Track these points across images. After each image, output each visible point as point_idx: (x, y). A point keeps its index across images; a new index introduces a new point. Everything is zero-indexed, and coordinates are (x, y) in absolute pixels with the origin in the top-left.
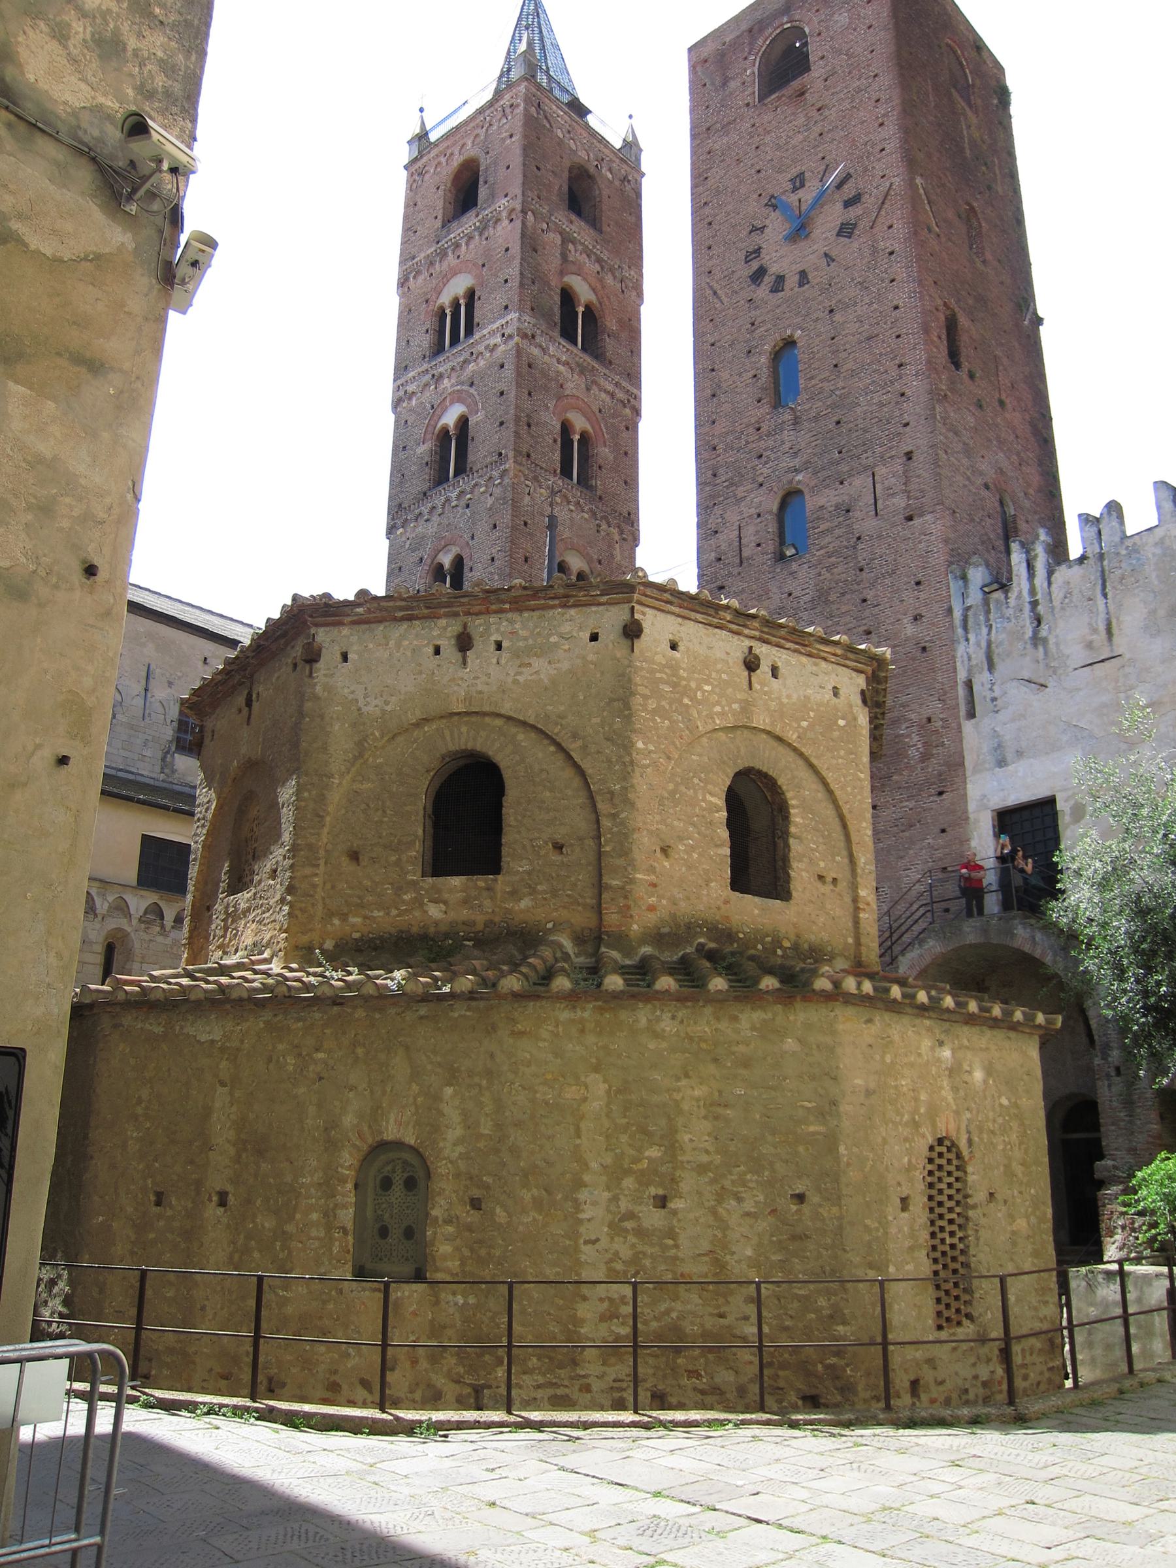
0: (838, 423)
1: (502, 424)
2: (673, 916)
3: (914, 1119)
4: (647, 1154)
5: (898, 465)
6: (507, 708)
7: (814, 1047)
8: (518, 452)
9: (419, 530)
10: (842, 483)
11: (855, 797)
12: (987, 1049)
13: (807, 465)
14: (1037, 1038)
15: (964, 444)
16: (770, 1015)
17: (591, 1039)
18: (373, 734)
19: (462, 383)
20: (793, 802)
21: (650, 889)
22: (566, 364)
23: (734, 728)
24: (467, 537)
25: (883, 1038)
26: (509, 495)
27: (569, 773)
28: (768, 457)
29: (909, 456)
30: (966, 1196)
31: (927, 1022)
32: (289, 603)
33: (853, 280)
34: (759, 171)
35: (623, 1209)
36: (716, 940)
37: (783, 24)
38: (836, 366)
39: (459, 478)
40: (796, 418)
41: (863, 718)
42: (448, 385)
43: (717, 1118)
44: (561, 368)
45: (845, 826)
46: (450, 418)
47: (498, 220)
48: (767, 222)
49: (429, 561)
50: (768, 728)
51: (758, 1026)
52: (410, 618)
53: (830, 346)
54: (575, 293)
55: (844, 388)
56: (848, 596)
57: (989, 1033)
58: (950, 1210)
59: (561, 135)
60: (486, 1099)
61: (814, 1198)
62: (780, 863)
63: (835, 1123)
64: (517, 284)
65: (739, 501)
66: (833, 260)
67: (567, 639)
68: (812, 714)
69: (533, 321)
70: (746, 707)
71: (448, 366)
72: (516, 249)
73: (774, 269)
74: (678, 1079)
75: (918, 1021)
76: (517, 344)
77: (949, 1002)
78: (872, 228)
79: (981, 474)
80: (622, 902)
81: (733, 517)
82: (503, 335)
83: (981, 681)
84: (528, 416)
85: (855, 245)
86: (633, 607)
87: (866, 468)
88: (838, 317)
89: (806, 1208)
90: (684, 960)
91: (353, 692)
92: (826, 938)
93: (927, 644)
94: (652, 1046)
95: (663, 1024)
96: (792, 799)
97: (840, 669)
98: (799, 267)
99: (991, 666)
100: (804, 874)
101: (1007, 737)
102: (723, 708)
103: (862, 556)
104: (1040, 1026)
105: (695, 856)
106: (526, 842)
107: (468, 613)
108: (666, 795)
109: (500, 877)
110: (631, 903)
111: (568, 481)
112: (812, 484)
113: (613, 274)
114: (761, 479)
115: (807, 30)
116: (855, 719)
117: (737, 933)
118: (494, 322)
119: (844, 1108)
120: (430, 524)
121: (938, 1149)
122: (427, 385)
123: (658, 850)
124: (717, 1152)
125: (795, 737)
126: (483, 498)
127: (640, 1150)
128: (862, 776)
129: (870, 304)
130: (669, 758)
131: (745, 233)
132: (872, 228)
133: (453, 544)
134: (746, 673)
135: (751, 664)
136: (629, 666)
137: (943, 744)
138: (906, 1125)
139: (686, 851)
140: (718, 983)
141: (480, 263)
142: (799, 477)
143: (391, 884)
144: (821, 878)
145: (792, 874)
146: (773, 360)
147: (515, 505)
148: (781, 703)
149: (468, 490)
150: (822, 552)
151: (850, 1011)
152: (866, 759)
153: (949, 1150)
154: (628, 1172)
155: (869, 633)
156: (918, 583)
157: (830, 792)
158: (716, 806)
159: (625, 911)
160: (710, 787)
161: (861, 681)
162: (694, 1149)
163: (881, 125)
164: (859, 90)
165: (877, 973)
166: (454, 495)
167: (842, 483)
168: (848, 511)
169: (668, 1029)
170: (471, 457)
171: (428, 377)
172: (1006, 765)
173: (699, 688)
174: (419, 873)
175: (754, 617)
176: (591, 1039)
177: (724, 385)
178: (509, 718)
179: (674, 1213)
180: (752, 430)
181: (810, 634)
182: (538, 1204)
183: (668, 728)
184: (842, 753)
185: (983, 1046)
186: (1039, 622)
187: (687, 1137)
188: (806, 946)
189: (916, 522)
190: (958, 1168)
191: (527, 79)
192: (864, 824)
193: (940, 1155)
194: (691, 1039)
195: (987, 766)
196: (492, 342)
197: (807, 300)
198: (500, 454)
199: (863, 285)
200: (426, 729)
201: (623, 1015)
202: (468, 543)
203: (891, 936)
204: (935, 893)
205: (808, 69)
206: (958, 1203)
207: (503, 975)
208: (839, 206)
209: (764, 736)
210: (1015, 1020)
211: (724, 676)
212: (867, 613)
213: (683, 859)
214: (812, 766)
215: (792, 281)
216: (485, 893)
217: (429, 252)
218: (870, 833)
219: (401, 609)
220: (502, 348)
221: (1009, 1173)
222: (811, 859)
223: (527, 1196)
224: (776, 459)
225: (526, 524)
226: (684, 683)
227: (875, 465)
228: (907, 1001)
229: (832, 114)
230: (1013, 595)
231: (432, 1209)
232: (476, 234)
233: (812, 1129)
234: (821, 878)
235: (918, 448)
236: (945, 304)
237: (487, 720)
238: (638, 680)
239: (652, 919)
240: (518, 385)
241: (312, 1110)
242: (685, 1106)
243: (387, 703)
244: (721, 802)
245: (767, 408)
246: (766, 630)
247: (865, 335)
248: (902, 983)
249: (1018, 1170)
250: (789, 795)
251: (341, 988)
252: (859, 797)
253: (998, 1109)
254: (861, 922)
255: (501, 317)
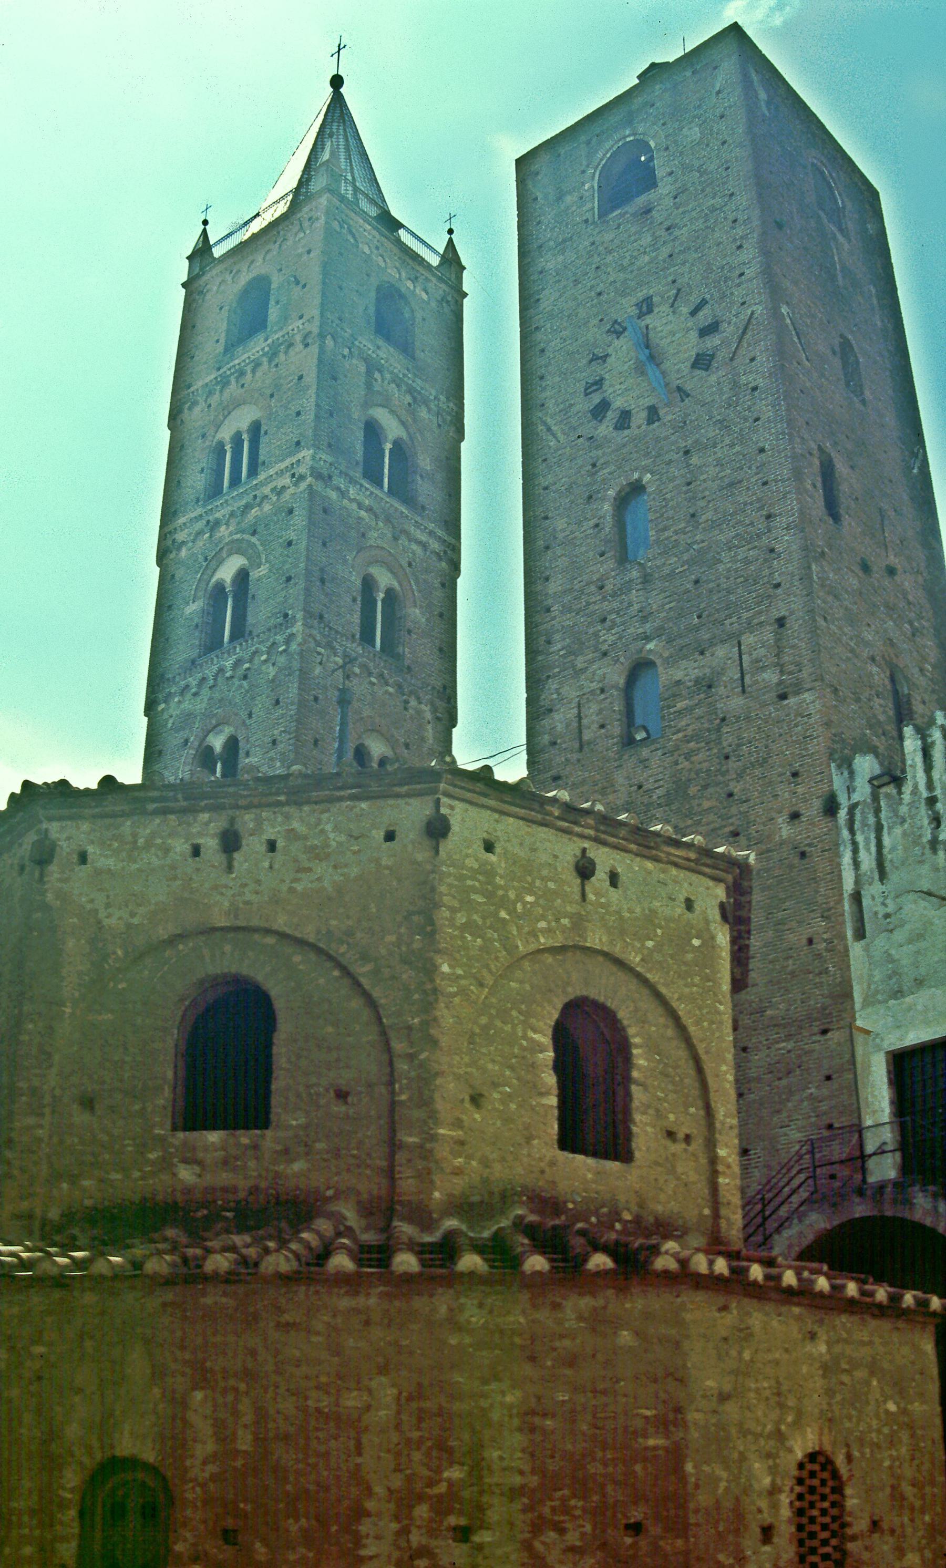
0: (697, 582)
1: (289, 579)
2: (485, 1181)
3: (779, 1431)
4: (446, 1475)
5: (768, 634)
6: (281, 922)
7: (655, 1340)
8: (308, 614)
9: (186, 705)
10: (702, 653)
11: (713, 1034)
12: (871, 1343)
13: (659, 633)
14: (931, 1329)
15: (846, 609)
16: (601, 1302)
17: (377, 1333)
18: (115, 953)
19: (243, 532)
20: (636, 1040)
21: (457, 1148)
22: (369, 510)
23: (563, 949)
24: (243, 714)
25: (741, 1330)
26: (296, 665)
27: (356, 1003)
28: (613, 621)
29: (781, 622)
30: (843, 1525)
31: (796, 1310)
32: (18, 790)
33: (710, 418)
34: (600, 294)
35: (414, 1545)
36: (541, 1213)
37: (625, 137)
38: (693, 515)
39: (235, 643)
40: (645, 576)
41: (723, 938)
42: (227, 533)
43: (533, 1430)
44: (363, 513)
45: (700, 1070)
46: (226, 573)
47: (291, 345)
48: (610, 350)
49: (197, 743)
50: (605, 949)
51: (586, 1315)
52: (164, 812)
53: (686, 493)
54: (381, 427)
55: (703, 541)
56: (711, 790)
57: (873, 1323)
58: (825, 1542)
59: (367, 250)
60: (245, 1406)
61: (655, 1530)
62: (620, 1116)
63: (681, 1435)
64: (312, 417)
65: (578, 673)
66: (688, 395)
67: (357, 838)
68: (659, 931)
69: (330, 459)
70: (579, 922)
71: (226, 511)
72: (311, 378)
73: (618, 403)
74: (485, 1382)
75: (784, 1309)
76: (310, 486)
77: (822, 1283)
78: (732, 359)
79: (867, 644)
80: (420, 1164)
81: (571, 692)
82: (293, 475)
83: (873, 892)
84: (322, 570)
85: (713, 379)
86: (439, 799)
87: (731, 636)
88: (694, 460)
89: (643, 1543)
90: (498, 1236)
91: (92, 901)
92: (676, 1210)
93: (807, 849)
94: (453, 1341)
95: (467, 1314)
96: (635, 1036)
97: (694, 877)
98: (648, 402)
99: (883, 874)
100: (649, 1129)
101: (904, 962)
102: (549, 922)
103: (728, 740)
104: (934, 1314)
105: (513, 1106)
106: (301, 1089)
107: (237, 807)
108: (477, 1031)
109: (269, 1133)
110: (432, 1165)
111: (371, 649)
112: (666, 654)
113: (427, 406)
114: (605, 647)
115: (652, 144)
116: (713, 938)
117: (565, 1202)
118: (282, 461)
119: (692, 1416)
120: (198, 699)
121: (809, 1467)
122: (200, 533)
123: (467, 1098)
124: (533, 1472)
125: (638, 959)
126: (264, 667)
127: (439, 1471)
128: (722, 1008)
129: (732, 446)
130: (481, 985)
131: (584, 361)
132: (732, 359)
133: (227, 723)
134: (579, 881)
135: (585, 870)
136: (433, 872)
137: (826, 971)
138: (769, 1437)
139: (502, 1101)
140: (537, 1263)
141: (269, 392)
142: (651, 646)
143: (134, 1139)
144: (670, 1135)
145: (635, 1129)
146: (618, 507)
147: (304, 675)
148: (621, 918)
149: (247, 657)
150: (680, 735)
151: (700, 1297)
152: (726, 987)
153: (823, 1468)
154: (421, 1498)
155: (736, 834)
156: (795, 775)
157: (681, 1028)
158: (539, 1044)
159: (425, 1176)
160: (533, 1021)
161: (720, 892)
162: (504, 1469)
163: (740, 247)
164: (713, 209)
165: (738, 1252)
166: (229, 663)
167: (702, 653)
168: (710, 687)
169: (473, 1319)
170: (250, 620)
171: (200, 525)
172: (903, 996)
173: (520, 898)
174: (168, 1125)
175: (587, 812)
176: (377, 1333)
177: (561, 536)
178: (283, 936)
179: (480, 1547)
180: (593, 588)
181: (657, 834)
182: (307, 1538)
183: (481, 949)
184: (697, 979)
185: (866, 1339)
186: (939, 825)
187: (496, 1454)
188: (651, 1219)
189: (792, 701)
190: (834, 1490)
191: (329, 191)
192: (724, 1068)
193: (812, 1474)
194: (502, 1332)
195: (880, 997)
196: (280, 483)
197: (657, 440)
198: (286, 615)
199: (724, 424)
200: (181, 947)
201: (419, 1303)
202: (244, 722)
203: (763, 1210)
204: (817, 1156)
205: (654, 185)
206: (834, 1534)
207: (267, 1251)
208: (694, 335)
209: (601, 959)
210: (904, 1306)
211: (551, 885)
212: (734, 810)
213: (498, 1110)
214: (658, 995)
215: (639, 418)
216: (250, 1153)
217: (208, 380)
218: (730, 1078)
219: (154, 800)
220: (292, 490)
221: (897, 1496)
222: (657, 1110)
223: (293, 1527)
224: (623, 623)
225: (316, 699)
226: (501, 893)
227: (741, 633)
228: (772, 1284)
229: (683, 233)
230: (907, 789)
231: (175, 1543)
232: (265, 359)
233: (651, 1442)
234: (670, 1135)
235: (792, 613)
236: (820, 448)
237: (256, 937)
238: (443, 889)
239: (458, 1185)
240: (310, 536)
241: (27, 1418)
242: (496, 1416)
243: (133, 915)
244: (545, 1039)
245: (611, 564)
246: (602, 828)
247: (727, 481)
248: (769, 1263)
249: (908, 1490)
250: (631, 1031)
251: (65, 1267)
252: (717, 1034)
253: (883, 1416)
254: (720, 1189)
255: (291, 454)
